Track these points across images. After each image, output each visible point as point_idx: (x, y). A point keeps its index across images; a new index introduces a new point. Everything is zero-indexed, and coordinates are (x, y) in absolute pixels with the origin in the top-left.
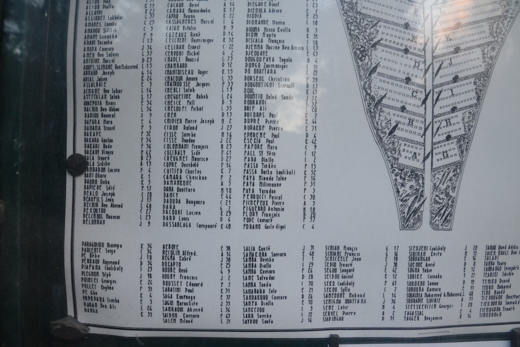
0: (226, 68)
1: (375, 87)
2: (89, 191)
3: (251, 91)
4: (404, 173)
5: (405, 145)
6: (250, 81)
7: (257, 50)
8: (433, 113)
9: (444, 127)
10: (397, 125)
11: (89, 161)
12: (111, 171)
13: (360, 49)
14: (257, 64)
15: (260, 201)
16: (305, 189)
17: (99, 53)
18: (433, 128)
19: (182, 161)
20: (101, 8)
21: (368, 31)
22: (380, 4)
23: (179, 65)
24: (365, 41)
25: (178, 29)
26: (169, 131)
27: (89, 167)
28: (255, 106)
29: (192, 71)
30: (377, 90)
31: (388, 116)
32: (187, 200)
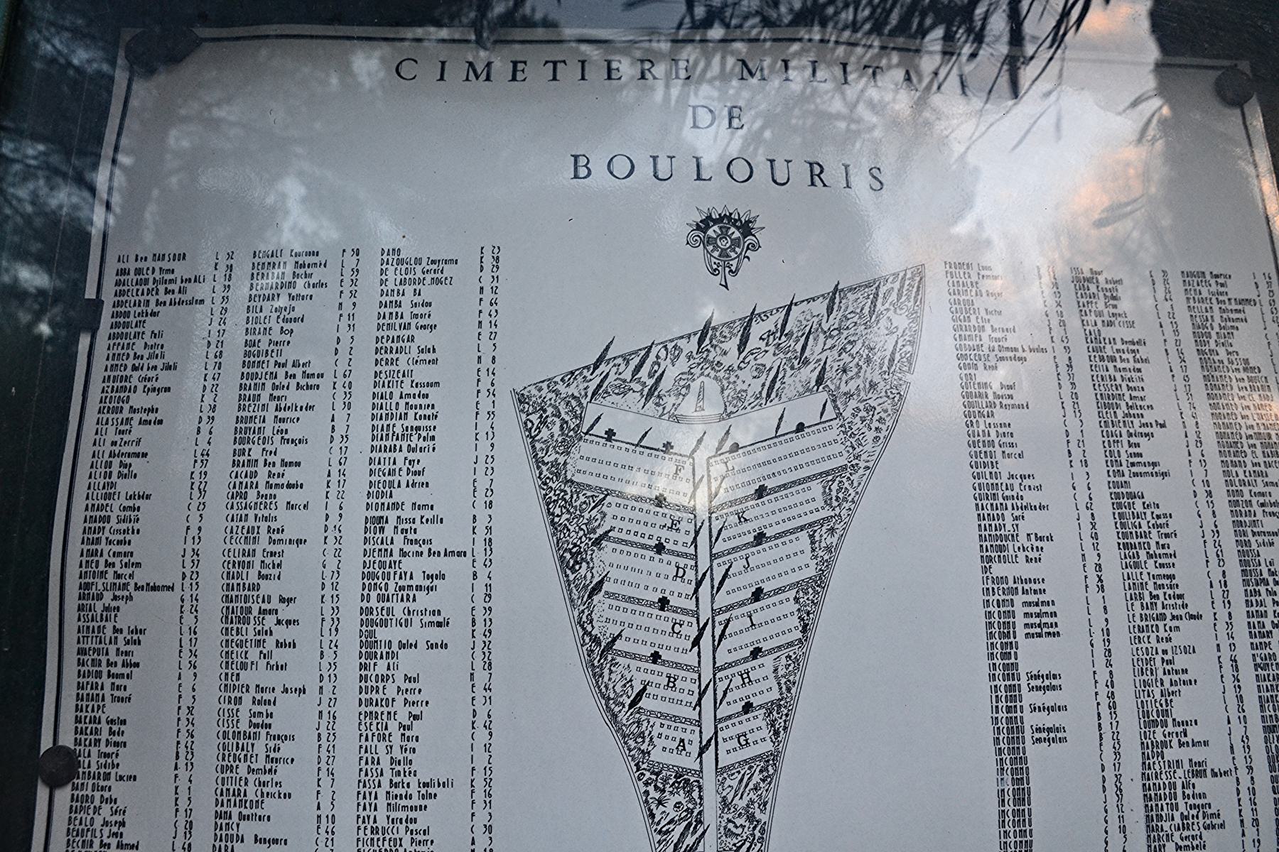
0: (328, 591)
1: (601, 619)
2: (79, 817)
3: (372, 634)
4: (662, 779)
5: (662, 725)
6: (370, 617)
7: (383, 559)
8: (715, 663)
9: (738, 688)
10: (644, 689)
11: (81, 759)
12: (121, 778)
13: (570, 550)
14: (383, 585)
15: (387, 839)
16: (473, 815)
17: (106, 561)
18: (715, 690)
19: (249, 763)
20: (114, 478)
21: (586, 515)
22: (609, 463)
23: (247, 586)
24: (581, 533)
25: (246, 520)
26: (226, 706)
27: (81, 770)
28: (379, 662)
29: (269, 597)
30: (604, 624)
31: (626, 673)
32: (256, 836)
